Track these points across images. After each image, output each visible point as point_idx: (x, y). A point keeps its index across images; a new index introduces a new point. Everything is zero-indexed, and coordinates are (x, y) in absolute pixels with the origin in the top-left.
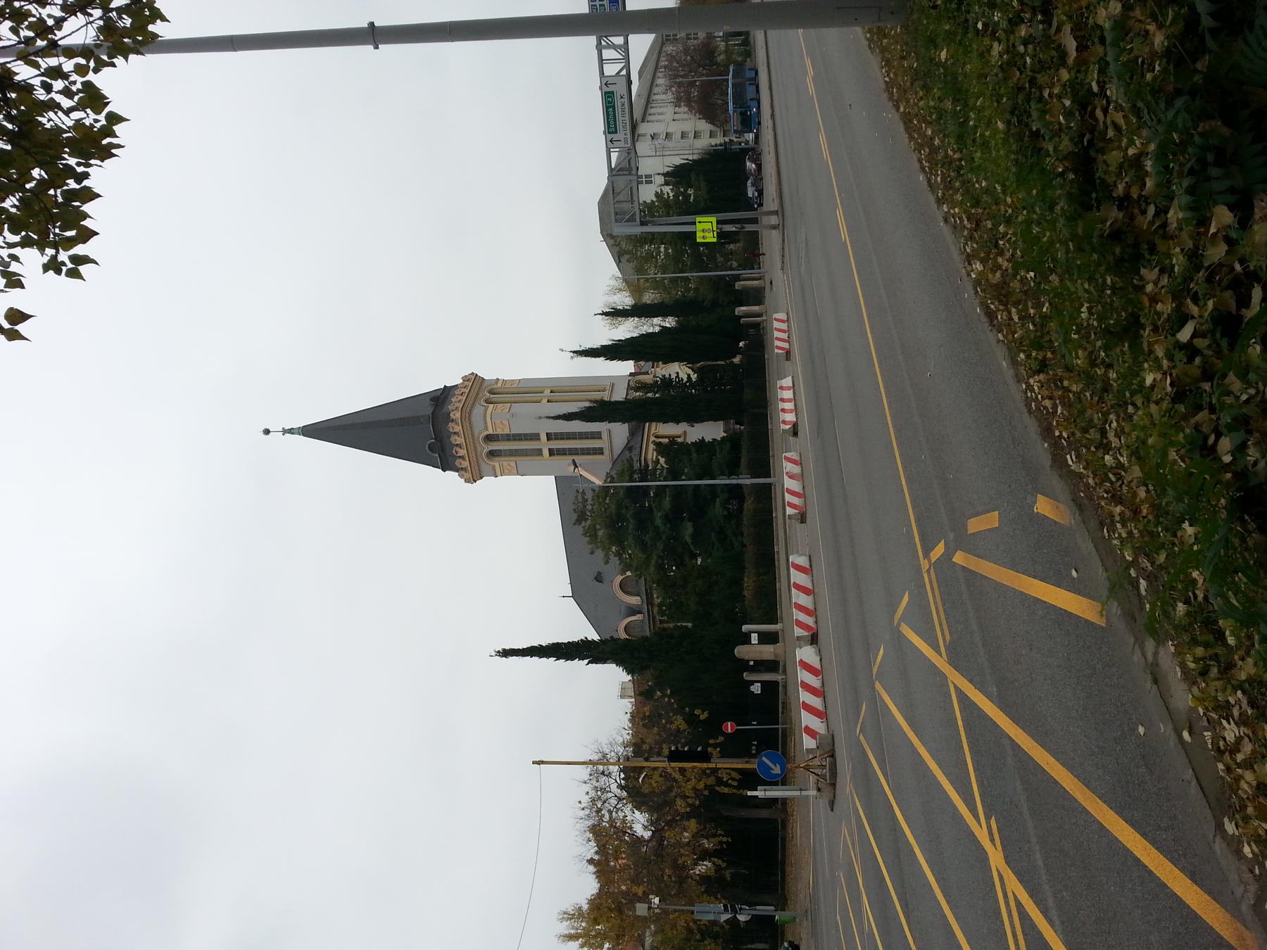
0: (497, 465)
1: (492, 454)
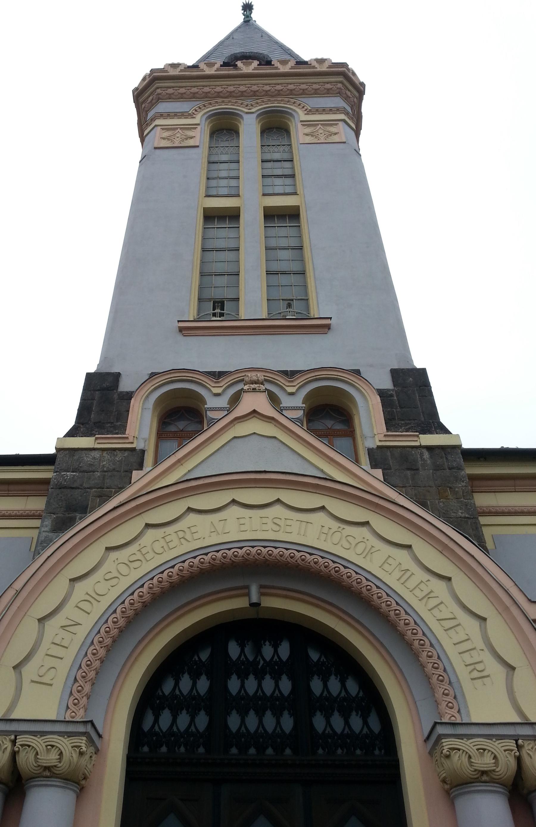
0: (197, 121)
1: (224, 128)
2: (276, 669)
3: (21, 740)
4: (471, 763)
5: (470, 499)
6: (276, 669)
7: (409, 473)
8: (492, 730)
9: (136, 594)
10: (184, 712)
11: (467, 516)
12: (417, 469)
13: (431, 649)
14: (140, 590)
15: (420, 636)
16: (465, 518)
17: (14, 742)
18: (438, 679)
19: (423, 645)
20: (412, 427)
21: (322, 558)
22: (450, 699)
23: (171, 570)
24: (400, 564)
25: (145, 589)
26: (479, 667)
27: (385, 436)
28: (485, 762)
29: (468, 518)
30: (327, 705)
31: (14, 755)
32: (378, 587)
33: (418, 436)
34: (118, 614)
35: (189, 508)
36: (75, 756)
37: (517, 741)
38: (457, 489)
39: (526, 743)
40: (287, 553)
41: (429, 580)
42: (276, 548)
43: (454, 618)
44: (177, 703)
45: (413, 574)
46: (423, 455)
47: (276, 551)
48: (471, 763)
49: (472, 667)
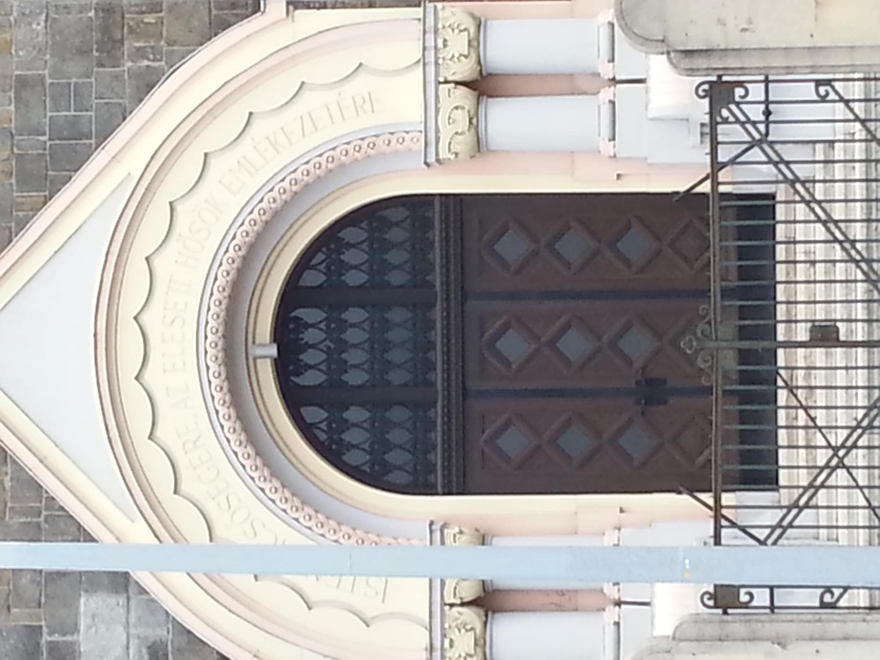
2: (336, 326)
3: (450, 599)
4: (462, 134)
5: (12, 7)
6: (336, 326)
8: (431, 107)
9: (273, 497)
10: (388, 436)
13: (338, 150)
14: (267, 491)
15: (323, 160)
16: (46, 21)
17: (452, 605)
18: (372, 149)
19: (333, 158)
21: (221, 264)
22: (394, 140)
23: (240, 455)
24: (230, 170)
25: (267, 486)
26: (359, 101)
28: (462, 119)
29: (47, 16)
30: (378, 267)
31: (463, 604)
32: (261, 201)
34: (300, 515)
35: (150, 438)
36: (464, 538)
37: (440, 83)
39: (441, 73)
40: (214, 309)
41: (253, 139)
42: (207, 323)
43: (302, 117)
44: (380, 445)
45: (244, 157)
47: (212, 323)
48: (462, 134)
49: (359, 109)
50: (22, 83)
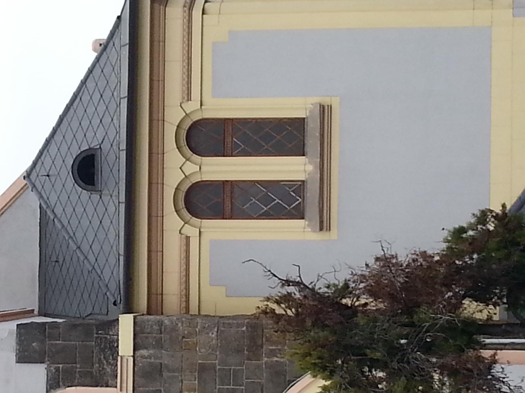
7: (165, 374)
11: (216, 330)
12: (161, 364)
16: (217, 332)
20: (104, 357)
27: (121, 390)
29: (218, 329)
33: (122, 357)
38: (186, 332)
46: (145, 356)
50: (203, 369)
